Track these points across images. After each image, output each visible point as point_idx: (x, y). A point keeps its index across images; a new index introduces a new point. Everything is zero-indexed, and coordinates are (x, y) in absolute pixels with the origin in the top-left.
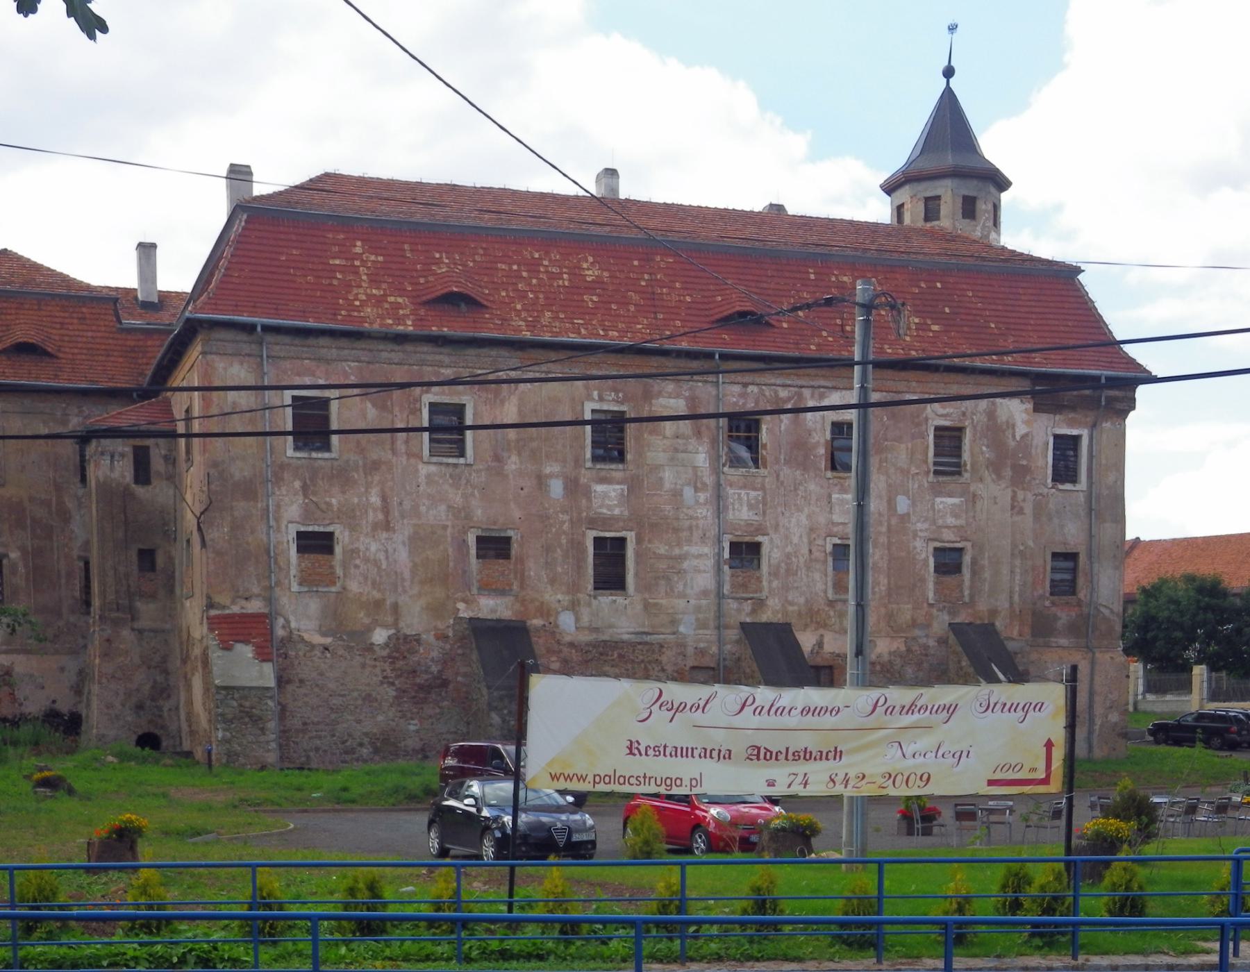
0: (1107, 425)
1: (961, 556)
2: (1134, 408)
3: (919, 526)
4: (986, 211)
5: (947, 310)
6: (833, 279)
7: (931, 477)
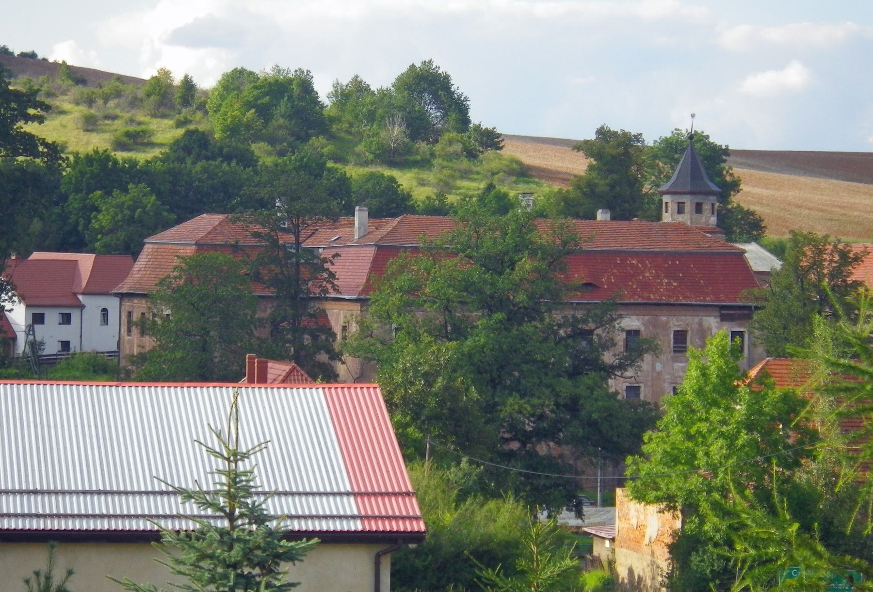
3: (667, 377)
7: (672, 354)
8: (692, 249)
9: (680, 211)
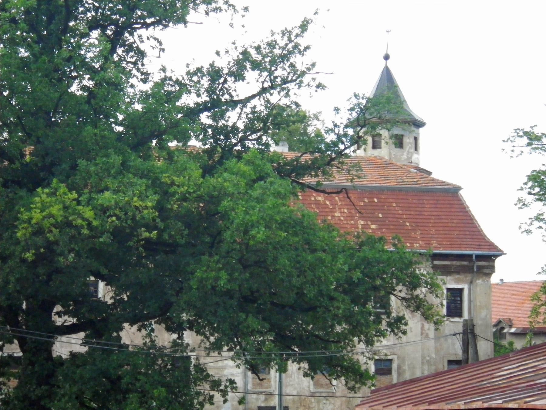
0: (479, 282)
1: (391, 364)
2: (494, 272)
4: (410, 143)
5: (380, 216)
6: (313, 199)
8: (393, 184)
9: (376, 146)
